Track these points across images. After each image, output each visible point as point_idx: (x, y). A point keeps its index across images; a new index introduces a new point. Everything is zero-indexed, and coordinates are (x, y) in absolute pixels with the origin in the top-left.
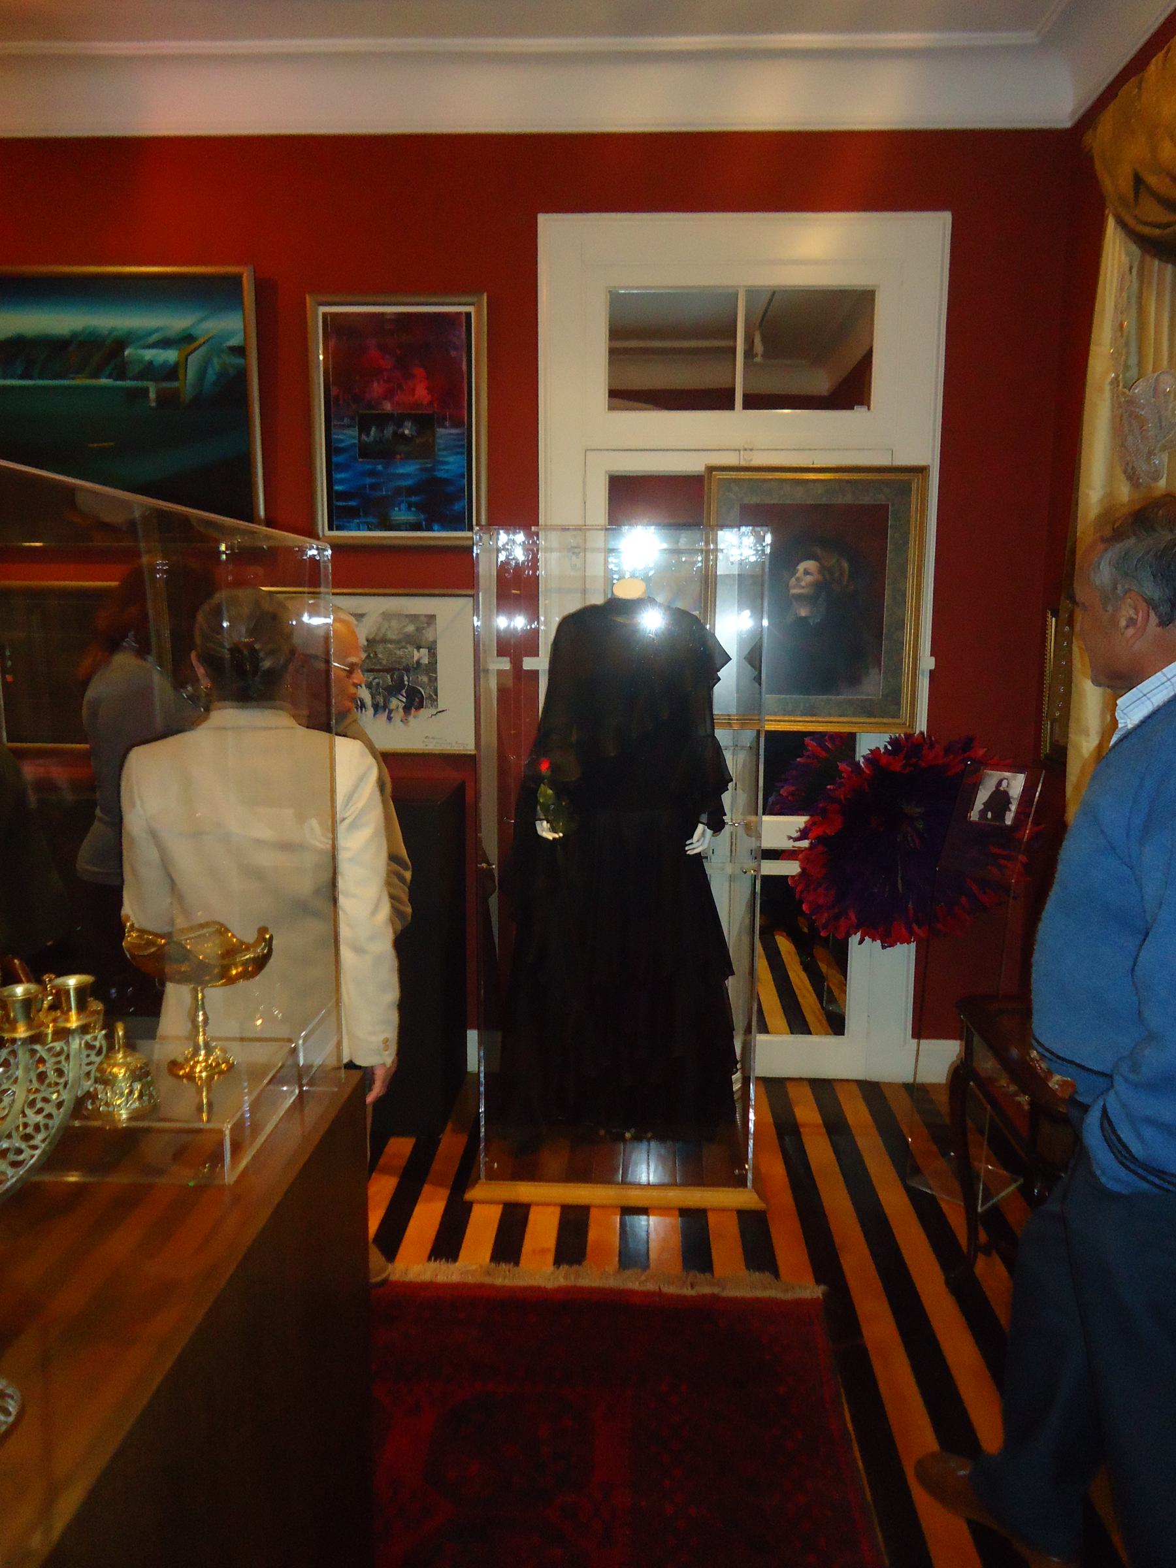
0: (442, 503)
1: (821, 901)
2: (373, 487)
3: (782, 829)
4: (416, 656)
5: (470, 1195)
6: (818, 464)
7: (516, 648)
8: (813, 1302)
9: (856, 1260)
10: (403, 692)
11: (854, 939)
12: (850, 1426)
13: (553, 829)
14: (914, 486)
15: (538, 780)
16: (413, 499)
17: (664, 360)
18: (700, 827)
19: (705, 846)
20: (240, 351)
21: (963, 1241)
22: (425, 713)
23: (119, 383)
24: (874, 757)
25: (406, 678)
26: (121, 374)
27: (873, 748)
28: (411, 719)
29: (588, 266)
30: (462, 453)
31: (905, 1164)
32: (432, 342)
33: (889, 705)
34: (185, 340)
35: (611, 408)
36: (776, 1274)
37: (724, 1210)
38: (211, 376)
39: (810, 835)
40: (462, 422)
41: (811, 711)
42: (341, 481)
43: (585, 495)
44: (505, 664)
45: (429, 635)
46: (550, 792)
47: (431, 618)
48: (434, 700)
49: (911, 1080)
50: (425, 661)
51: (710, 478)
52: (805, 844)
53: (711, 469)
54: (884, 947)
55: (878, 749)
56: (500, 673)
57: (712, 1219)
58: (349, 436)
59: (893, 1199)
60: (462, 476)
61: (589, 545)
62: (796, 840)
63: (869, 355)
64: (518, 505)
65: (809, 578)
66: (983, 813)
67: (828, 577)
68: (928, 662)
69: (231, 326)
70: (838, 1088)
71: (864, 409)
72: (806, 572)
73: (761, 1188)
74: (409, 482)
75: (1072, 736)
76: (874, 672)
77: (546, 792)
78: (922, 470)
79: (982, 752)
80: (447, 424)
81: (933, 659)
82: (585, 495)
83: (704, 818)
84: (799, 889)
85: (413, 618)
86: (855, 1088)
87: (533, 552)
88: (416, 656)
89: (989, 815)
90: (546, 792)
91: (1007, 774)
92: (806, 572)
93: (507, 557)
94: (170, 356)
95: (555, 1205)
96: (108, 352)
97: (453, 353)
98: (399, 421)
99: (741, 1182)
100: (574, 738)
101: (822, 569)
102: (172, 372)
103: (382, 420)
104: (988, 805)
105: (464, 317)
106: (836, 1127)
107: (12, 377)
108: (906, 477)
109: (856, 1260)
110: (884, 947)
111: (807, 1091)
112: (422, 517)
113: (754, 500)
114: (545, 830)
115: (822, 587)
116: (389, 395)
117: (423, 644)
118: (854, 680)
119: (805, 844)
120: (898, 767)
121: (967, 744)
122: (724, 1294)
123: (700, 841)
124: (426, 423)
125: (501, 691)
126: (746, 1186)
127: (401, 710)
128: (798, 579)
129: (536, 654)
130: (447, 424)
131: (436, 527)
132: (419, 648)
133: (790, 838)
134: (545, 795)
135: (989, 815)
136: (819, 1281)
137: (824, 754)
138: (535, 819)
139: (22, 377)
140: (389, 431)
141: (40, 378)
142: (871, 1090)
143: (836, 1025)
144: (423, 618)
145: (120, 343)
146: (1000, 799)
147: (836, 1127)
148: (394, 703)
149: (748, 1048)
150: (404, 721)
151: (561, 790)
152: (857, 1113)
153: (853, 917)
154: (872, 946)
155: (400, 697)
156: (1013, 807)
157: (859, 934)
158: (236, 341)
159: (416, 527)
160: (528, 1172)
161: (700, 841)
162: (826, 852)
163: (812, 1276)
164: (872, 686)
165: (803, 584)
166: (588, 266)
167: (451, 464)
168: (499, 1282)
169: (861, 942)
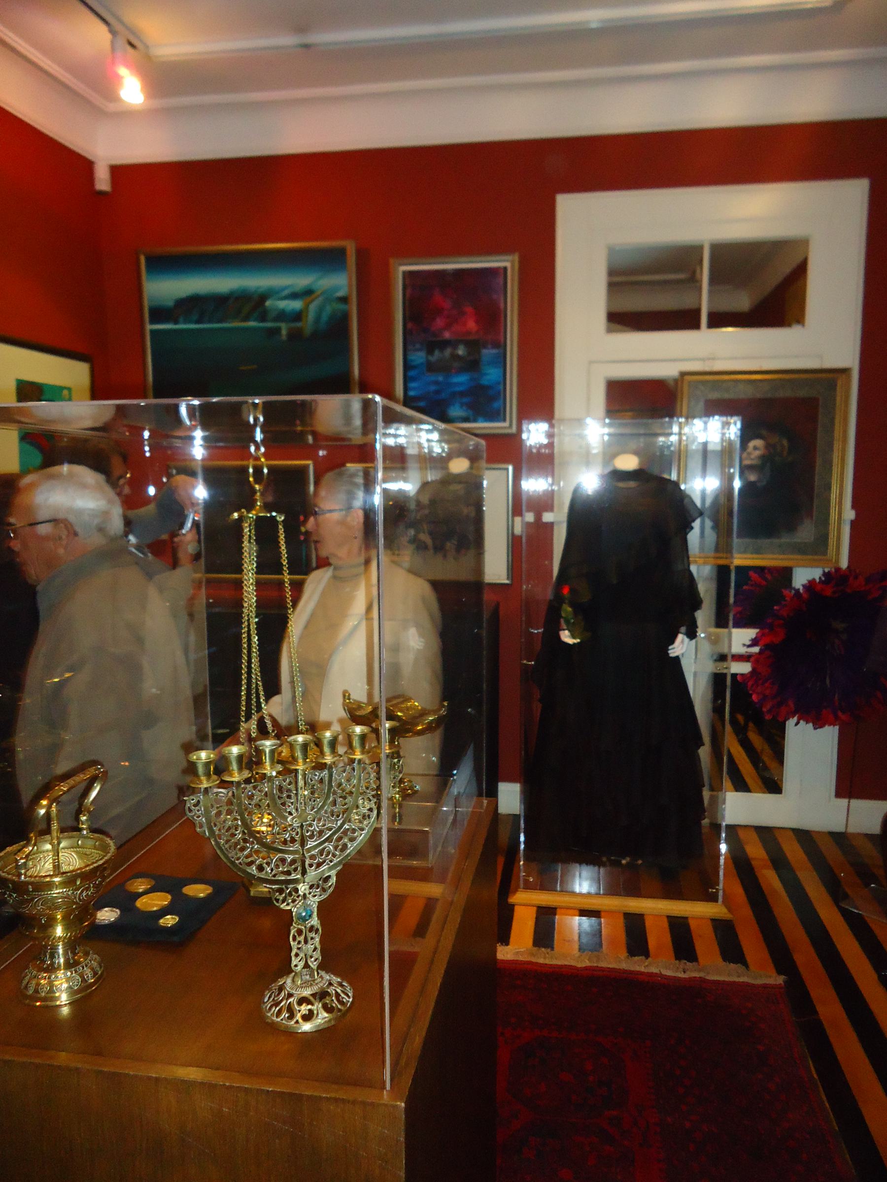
1: (767, 692)
2: (437, 392)
3: (741, 639)
5: (512, 900)
7: (544, 503)
8: (779, 986)
9: (805, 956)
11: (791, 723)
12: (815, 1076)
13: (573, 637)
14: (839, 383)
17: (650, 294)
18: (680, 637)
19: (684, 650)
20: (344, 300)
23: (261, 325)
24: (811, 586)
26: (263, 318)
29: (593, 231)
31: (836, 892)
32: (478, 288)
33: (819, 547)
34: (307, 293)
35: (609, 330)
36: (747, 967)
37: (701, 918)
38: (325, 317)
40: (500, 345)
41: (758, 551)
42: (414, 389)
46: (570, 609)
49: (840, 828)
52: (756, 650)
53: (683, 374)
54: (815, 729)
58: (419, 357)
59: (829, 914)
62: (749, 646)
64: (540, 400)
65: (757, 453)
68: (849, 514)
69: (339, 282)
70: (777, 833)
74: (461, 389)
77: (567, 609)
80: (490, 346)
83: (683, 629)
84: (750, 683)
86: (791, 833)
90: (567, 609)
92: (755, 448)
94: (296, 305)
96: (252, 304)
97: (495, 297)
98: (453, 344)
99: (713, 898)
101: (768, 446)
102: (298, 316)
103: (443, 345)
105: (502, 271)
106: (779, 862)
107: (190, 322)
108: (829, 379)
109: (805, 956)
110: (815, 729)
111: (754, 836)
113: (715, 395)
114: (566, 637)
115: (766, 460)
116: (448, 326)
118: (791, 528)
119: (756, 650)
120: (829, 592)
122: (707, 978)
123: (680, 647)
124: (474, 346)
126: (716, 901)
128: (749, 454)
133: (744, 645)
136: (779, 972)
139: (198, 322)
140: (448, 352)
141: (210, 322)
142: (803, 836)
143: (774, 787)
145: (262, 297)
147: (779, 862)
148: (448, 545)
149: (714, 801)
151: (578, 608)
152: (794, 852)
153: (792, 706)
154: (806, 728)
157: (796, 719)
158: (341, 294)
161: (680, 647)
162: (771, 658)
163: (774, 971)
164: (806, 532)
165: (752, 457)
166: (593, 231)
167: (491, 375)
168: (541, 961)
169: (797, 724)
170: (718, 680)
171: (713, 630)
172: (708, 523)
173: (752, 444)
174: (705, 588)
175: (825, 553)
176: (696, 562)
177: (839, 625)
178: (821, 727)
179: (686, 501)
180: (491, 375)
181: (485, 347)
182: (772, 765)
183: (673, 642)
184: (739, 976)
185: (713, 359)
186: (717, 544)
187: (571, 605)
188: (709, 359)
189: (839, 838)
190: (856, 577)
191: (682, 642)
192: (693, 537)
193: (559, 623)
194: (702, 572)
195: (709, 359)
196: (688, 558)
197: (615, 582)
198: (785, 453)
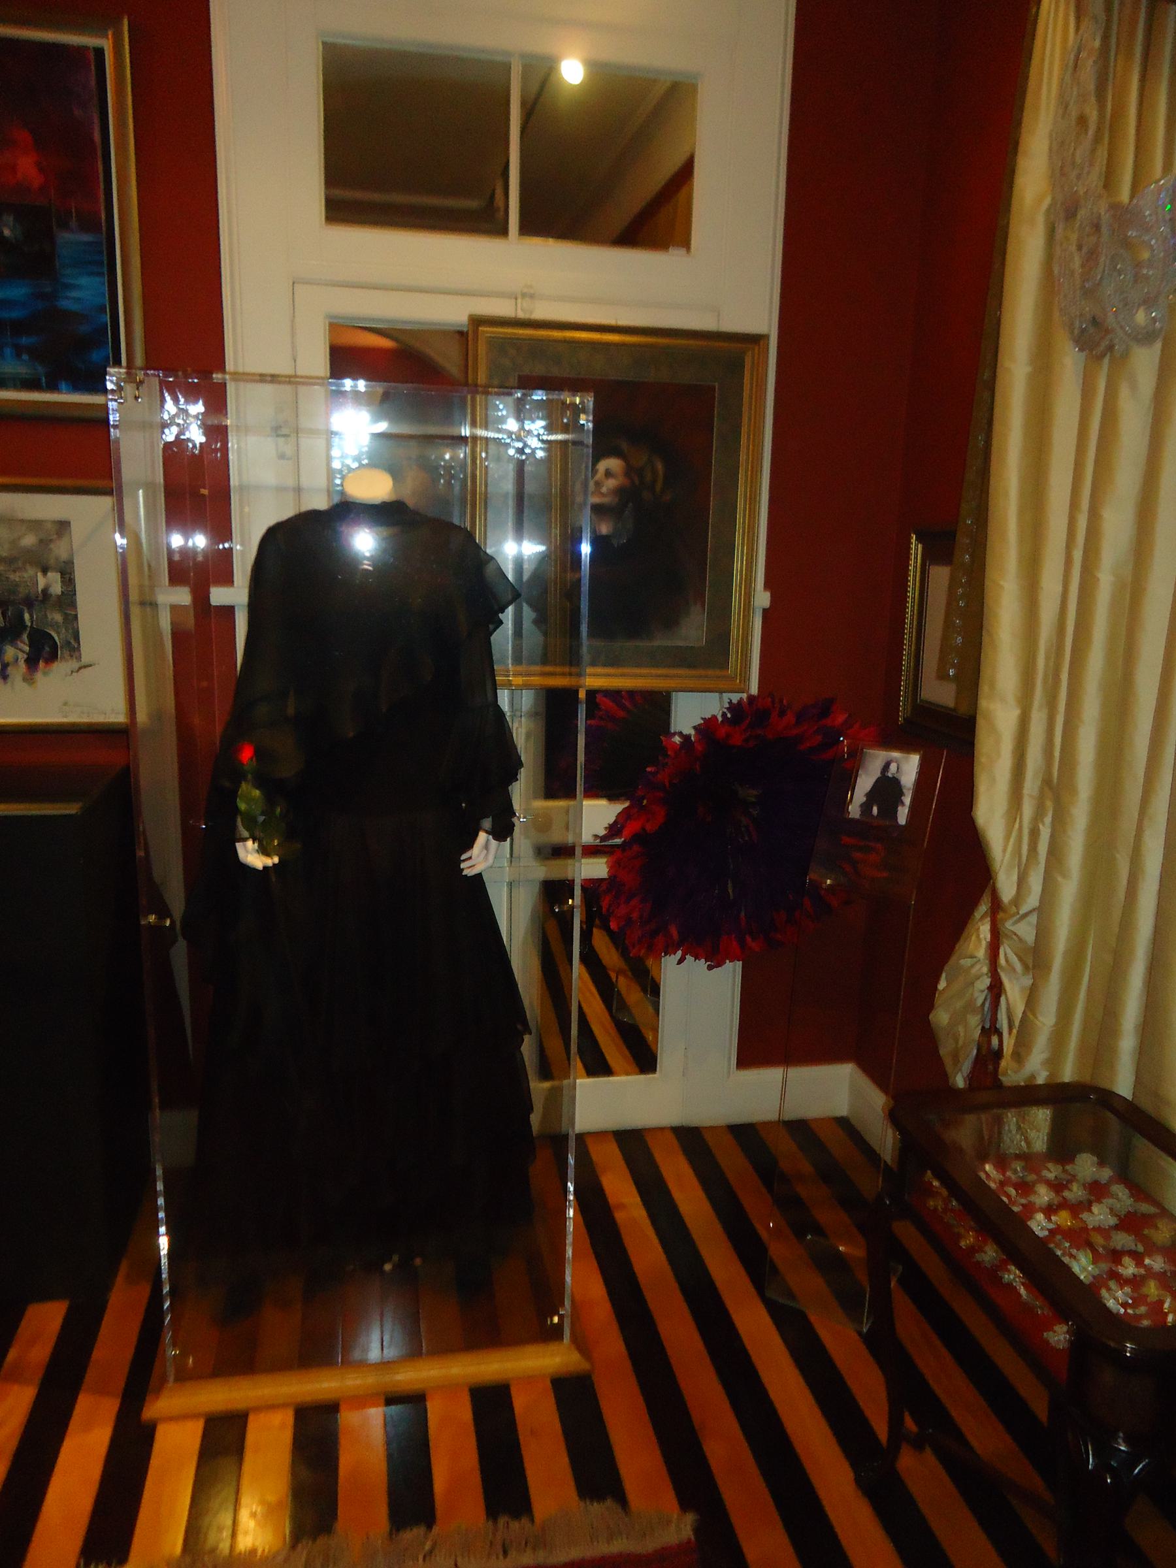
0: (78, 355)
4: (42, 582)
6: (623, 322)
7: (199, 574)
10: (25, 637)
13: (264, 851)
15: (238, 776)
16: (24, 340)
18: (482, 837)
21: (881, 1430)
22: (61, 667)
24: (707, 727)
25: (27, 616)
27: (708, 716)
28: (39, 676)
30: (101, 274)
33: (712, 657)
36: (622, 1500)
39: (624, 833)
40: (99, 226)
43: (294, 347)
44: (183, 596)
45: (60, 550)
46: (257, 793)
47: (63, 526)
48: (73, 647)
50: (57, 589)
51: (476, 332)
53: (477, 321)
55: (714, 717)
56: (174, 608)
57: (520, 1401)
60: (102, 309)
61: (304, 423)
63: (685, 173)
64: (192, 351)
65: (611, 483)
66: (866, 807)
67: (637, 482)
68: (762, 599)
70: (649, 1139)
71: (683, 251)
72: (608, 474)
73: (581, 1344)
74: (15, 314)
75: (983, 703)
76: (695, 610)
77: (250, 796)
78: (756, 340)
79: (841, 718)
81: (768, 594)
82: (294, 347)
83: (487, 823)
85: (35, 525)
87: (217, 433)
88: (42, 582)
89: (875, 810)
90: (250, 796)
91: (896, 754)
92: (608, 474)
93: (177, 436)
95: (284, 1406)
100: (291, 711)
101: (629, 471)
104: (873, 795)
105: (92, 55)
108: (728, 351)
110: (710, 968)
112: (41, 369)
114: (251, 855)
117: (52, 562)
118: (671, 623)
121: (825, 708)
125: (178, 636)
127: (22, 664)
129: (227, 579)
130: (73, 223)
131: (63, 386)
132: (45, 571)
133: (596, 836)
134: (249, 800)
135: (875, 810)
137: (622, 714)
138: (233, 839)
142: (690, 1139)
143: (645, 1060)
144: (49, 526)
146: (887, 789)
150: (29, 679)
151: (271, 787)
154: (696, 967)
155: (21, 645)
156: (907, 800)
157: (679, 953)
159: (31, 384)
160: (240, 1360)
161: (483, 856)
164: (693, 630)
167: (83, 291)
169: (680, 962)
170: (554, 891)
171: (540, 804)
172: (528, 614)
173: (603, 465)
174: (524, 733)
175: (724, 665)
176: (508, 685)
177: (751, 794)
178: (719, 964)
179: (490, 569)
180: (83, 291)
181: (64, 225)
182: (632, 994)
183: (470, 846)
184: (610, 1538)
185: (532, 296)
186: (545, 647)
187: (261, 781)
188: (524, 295)
189: (745, 1134)
190: (782, 713)
191: (486, 846)
192: (503, 638)
193: (234, 828)
194: (517, 703)
195: (524, 295)
196: (493, 676)
197: (351, 734)
198: (659, 486)
